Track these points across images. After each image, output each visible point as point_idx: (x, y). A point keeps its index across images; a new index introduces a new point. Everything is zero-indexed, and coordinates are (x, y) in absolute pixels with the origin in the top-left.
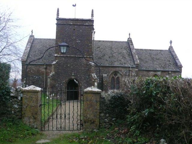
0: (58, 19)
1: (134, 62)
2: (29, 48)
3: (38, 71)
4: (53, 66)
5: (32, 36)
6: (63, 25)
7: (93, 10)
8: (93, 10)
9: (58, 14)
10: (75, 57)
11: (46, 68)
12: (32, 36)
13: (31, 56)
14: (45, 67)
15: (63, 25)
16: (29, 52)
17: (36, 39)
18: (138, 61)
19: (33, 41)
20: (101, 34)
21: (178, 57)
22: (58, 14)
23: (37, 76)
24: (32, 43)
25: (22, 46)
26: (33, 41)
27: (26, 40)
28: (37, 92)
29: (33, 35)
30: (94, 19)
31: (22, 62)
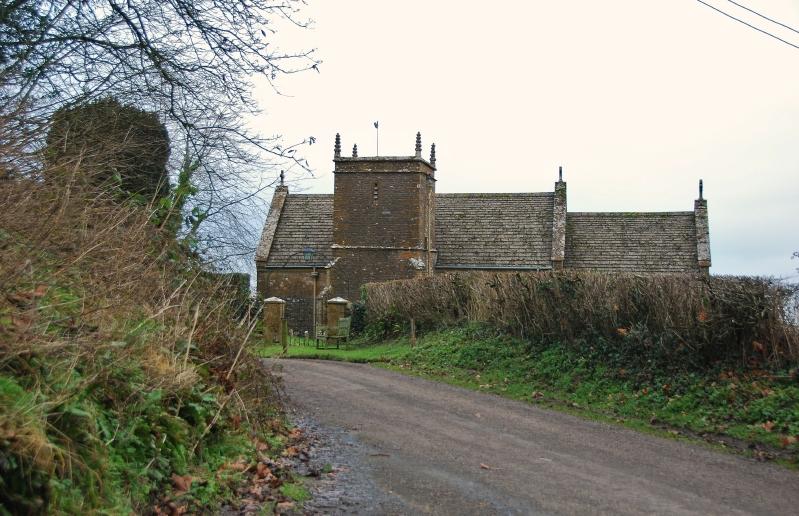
0: (340, 162)
1: (779, 484)
2: (275, 225)
3: (298, 284)
4: (328, 272)
5: (282, 189)
6: (348, 168)
7: (419, 135)
8: (419, 135)
9: (338, 150)
10: (380, 249)
11: (317, 278)
12: (282, 189)
13: (279, 247)
14: (314, 273)
15: (348, 168)
16: (274, 236)
17: (294, 196)
18: (563, 253)
19: (286, 203)
20: (446, 183)
21: (761, 275)
22: (338, 150)
23: (295, 297)
24: (283, 210)
25: (257, 220)
26: (286, 203)
27: (269, 195)
28: (279, 303)
29: (285, 184)
30: (437, 164)
31: (258, 262)
